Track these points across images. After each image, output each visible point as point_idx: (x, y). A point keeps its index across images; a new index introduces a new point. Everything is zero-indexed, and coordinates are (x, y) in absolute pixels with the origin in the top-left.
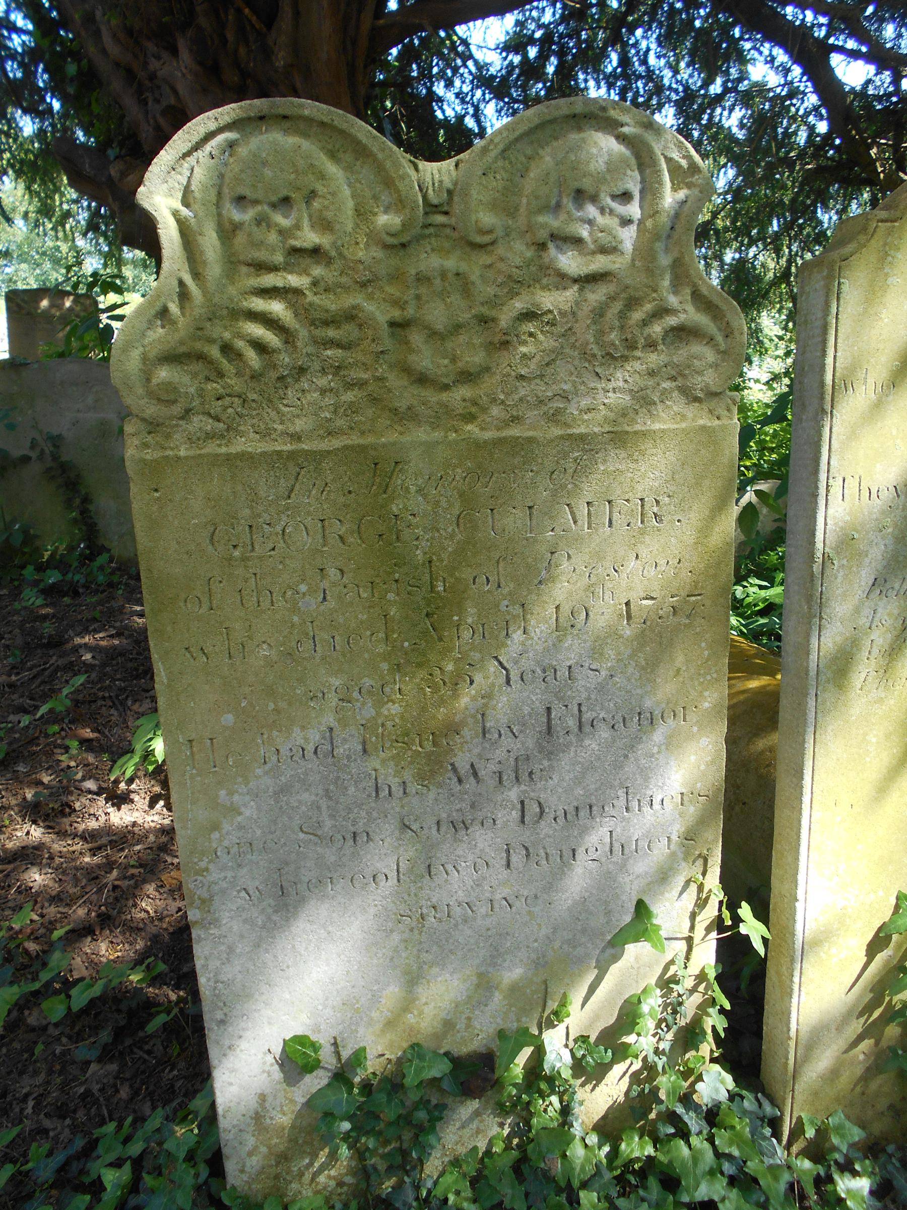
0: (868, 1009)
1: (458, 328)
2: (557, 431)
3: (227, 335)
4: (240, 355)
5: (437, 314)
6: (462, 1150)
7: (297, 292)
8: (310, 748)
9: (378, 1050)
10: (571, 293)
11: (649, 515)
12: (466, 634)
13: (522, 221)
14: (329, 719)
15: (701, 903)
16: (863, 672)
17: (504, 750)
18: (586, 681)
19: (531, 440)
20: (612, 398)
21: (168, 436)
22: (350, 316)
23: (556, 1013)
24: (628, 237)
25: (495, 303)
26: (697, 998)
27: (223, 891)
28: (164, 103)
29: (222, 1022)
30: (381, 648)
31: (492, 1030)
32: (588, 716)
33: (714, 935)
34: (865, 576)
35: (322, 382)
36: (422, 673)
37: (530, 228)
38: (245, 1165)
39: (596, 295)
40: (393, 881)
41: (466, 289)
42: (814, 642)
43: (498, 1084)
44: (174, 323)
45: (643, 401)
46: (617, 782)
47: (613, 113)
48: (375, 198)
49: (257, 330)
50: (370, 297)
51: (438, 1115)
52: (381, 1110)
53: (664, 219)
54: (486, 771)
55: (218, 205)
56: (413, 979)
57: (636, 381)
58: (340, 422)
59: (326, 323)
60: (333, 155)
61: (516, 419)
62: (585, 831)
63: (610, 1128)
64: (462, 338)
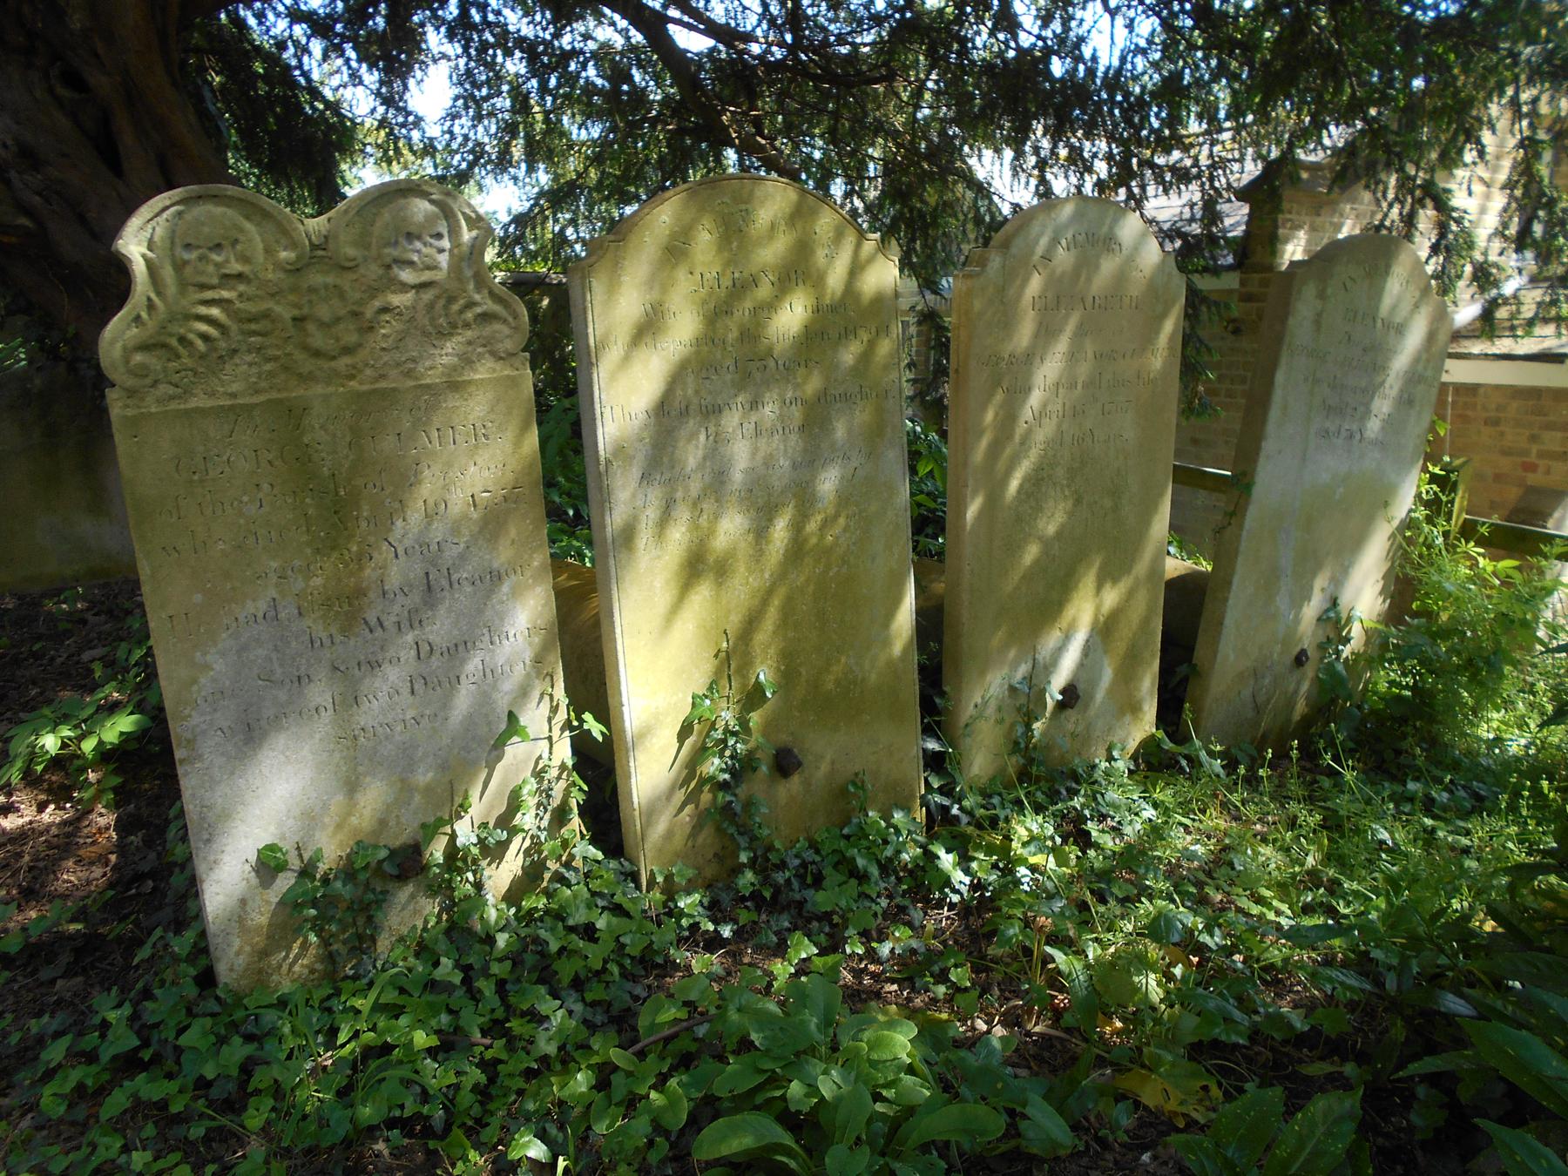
0: (686, 782)
1: (338, 320)
2: (412, 383)
3: (182, 331)
4: (191, 344)
5: (324, 312)
6: (405, 931)
7: (228, 301)
8: (260, 615)
9: (331, 850)
10: (411, 295)
11: (479, 436)
12: (364, 524)
13: (374, 252)
14: (273, 593)
15: (554, 710)
16: (644, 537)
17: (396, 610)
18: (451, 552)
19: (394, 390)
20: (445, 360)
21: (142, 399)
22: (267, 315)
23: (461, 806)
24: (443, 260)
25: (361, 302)
26: (562, 784)
27: (204, 732)
29: (209, 841)
30: (304, 538)
31: (416, 825)
32: (455, 577)
33: (567, 733)
34: (635, 472)
35: (249, 358)
36: (335, 555)
37: (379, 256)
38: (232, 961)
39: (428, 296)
40: (330, 711)
41: (342, 295)
42: (608, 521)
43: (425, 868)
44: (143, 324)
45: (467, 361)
46: (479, 627)
47: (425, 188)
48: (277, 242)
49: (203, 327)
50: (278, 303)
51: (382, 900)
52: (335, 903)
53: (465, 249)
54: (389, 622)
55: (172, 249)
56: (352, 787)
57: (460, 349)
58: (263, 384)
59: (250, 321)
60: (247, 218)
61: (383, 377)
62: (463, 661)
63: (513, 896)
64: (342, 326)
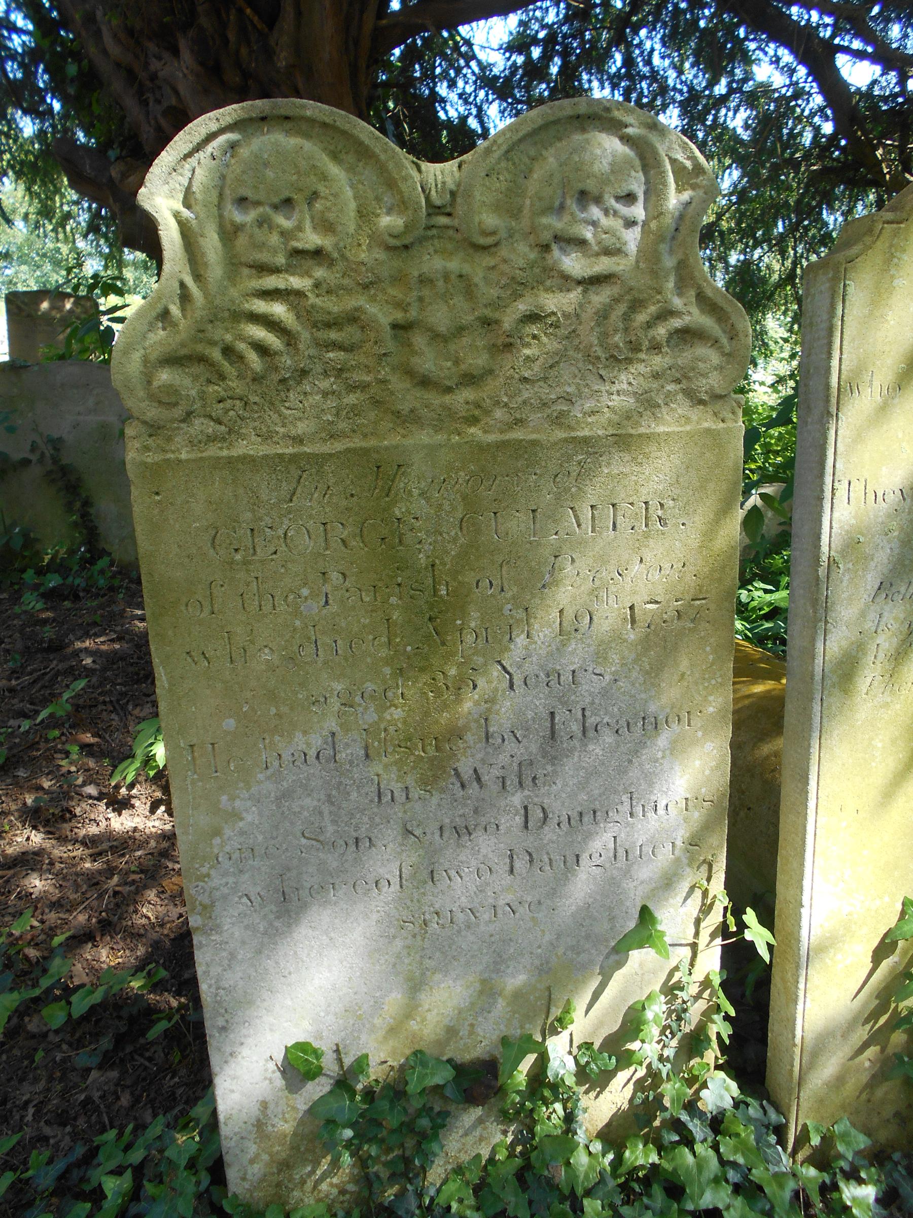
0: (874, 1015)
1: (461, 330)
2: (561, 434)
3: (228, 337)
4: (241, 358)
5: (440, 316)
6: (465, 1158)
7: (299, 294)
8: (312, 753)
9: (381, 1057)
10: (575, 295)
11: (654, 519)
12: (470, 638)
13: (525, 222)
14: (331, 724)
15: (706, 909)
16: (869, 676)
17: (508, 755)
18: (590, 686)
19: (534, 443)
20: (616, 401)
21: (169, 439)
22: (352, 318)
23: (560, 1020)
24: (632, 238)
25: (498, 305)
26: (702, 1005)
27: (225, 897)
28: (165, 104)
29: (224, 1029)
30: (383, 653)
31: (495, 1036)
32: (592, 721)
33: (719, 941)
34: (871, 580)
35: (325, 384)
36: (425, 678)
37: (533, 230)
38: (246, 1173)
39: (600, 297)
40: (395, 887)
41: (469, 291)
42: (820, 646)
43: (501, 1092)
44: (175, 325)
45: (648, 403)
46: (621, 787)
47: (617, 114)
48: (378, 199)
49: (259, 333)
50: (373, 299)
51: (441, 1123)
52: (383, 1117)
53: (668, 221)
54: (490, 776)
55: (219, 206)
56: (415, 986)
57: (640, 384)
58: (342, 425)
59: (328, 325)
60: (335, 156)
61: (519, 422)
62: (588, 836)
63: (614, 1136)
64: (465, 340)
